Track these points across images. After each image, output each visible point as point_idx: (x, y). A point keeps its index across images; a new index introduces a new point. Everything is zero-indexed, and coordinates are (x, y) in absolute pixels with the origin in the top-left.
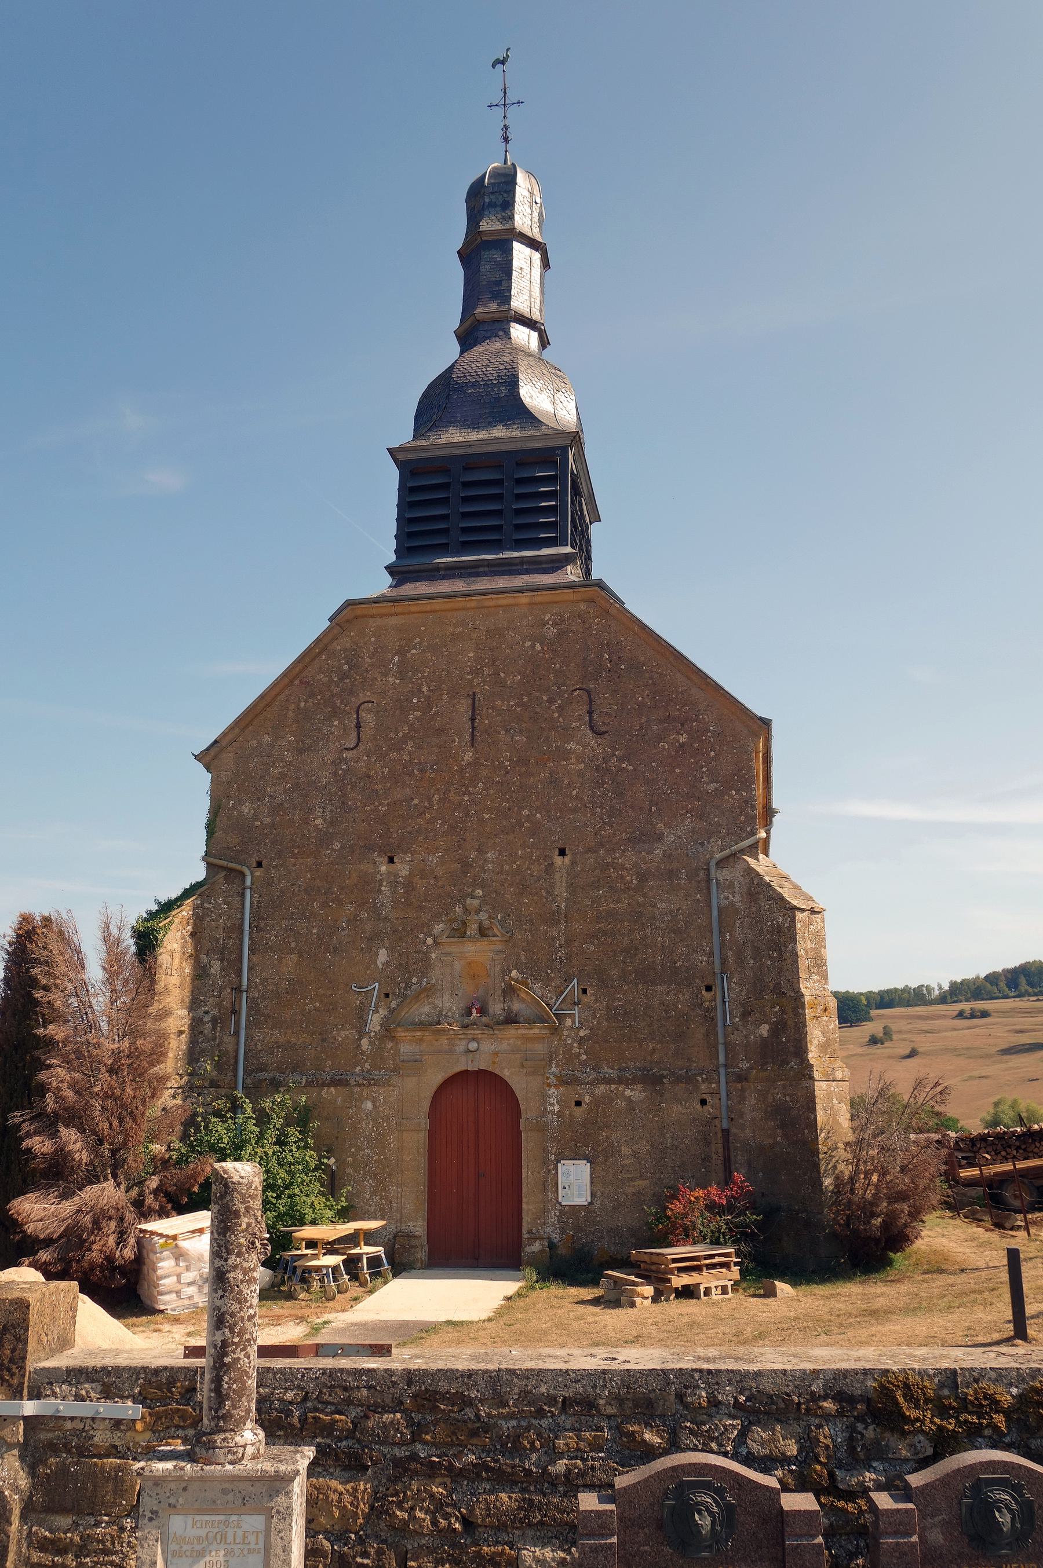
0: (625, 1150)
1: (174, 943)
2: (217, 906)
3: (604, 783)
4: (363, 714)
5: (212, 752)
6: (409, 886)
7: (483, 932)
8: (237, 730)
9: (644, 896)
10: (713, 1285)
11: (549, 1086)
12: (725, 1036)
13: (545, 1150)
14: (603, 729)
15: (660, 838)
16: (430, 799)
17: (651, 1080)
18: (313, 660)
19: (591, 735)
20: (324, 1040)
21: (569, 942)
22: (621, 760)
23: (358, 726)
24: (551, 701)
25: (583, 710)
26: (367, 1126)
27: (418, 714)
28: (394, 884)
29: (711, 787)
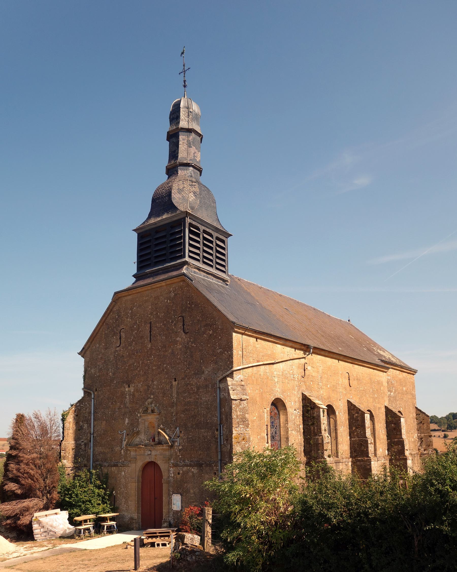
0: (192, 491)
1: (70, 419)
3: (187, 352)
4: (121, 333)
5: (83, 352)
6: (134, 395)
7: (153, 411)
8: (89, 343)
9: (199, 395)
10: (160, 543)
11: (171, 467)
14: (187, 331)
15: (203, 372)
16: (139, 363)
17: (199, 465)
18: (108, 315)
19: (184, 334)
20: (112, 451)
21: (177, 414)
23: (120, 338)
24: (172, 322)
25: (181, 324)
26: (123, 480)
27: (136, 331)
28: (130, 395)
29: (219, 351)
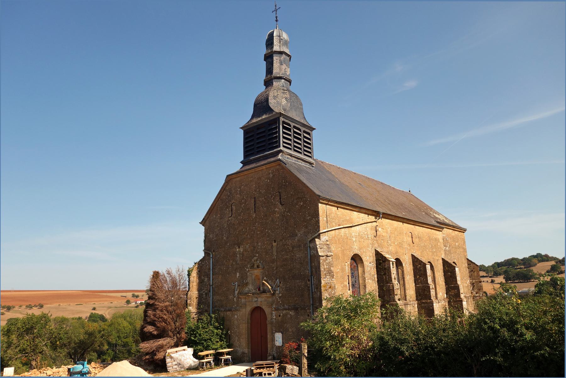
0: (290, 330)
1: (194, 274)
2: (206, 263)
6: (243, 254)
7: (258, 267)
12: (312, 295)
13: (272, 329)
15: (297, 235)
17: (296, 309)
21: (277, 268)
22: (287, 212)
26: (236, 322)
28: (240, 254)
29: (308, 218)
